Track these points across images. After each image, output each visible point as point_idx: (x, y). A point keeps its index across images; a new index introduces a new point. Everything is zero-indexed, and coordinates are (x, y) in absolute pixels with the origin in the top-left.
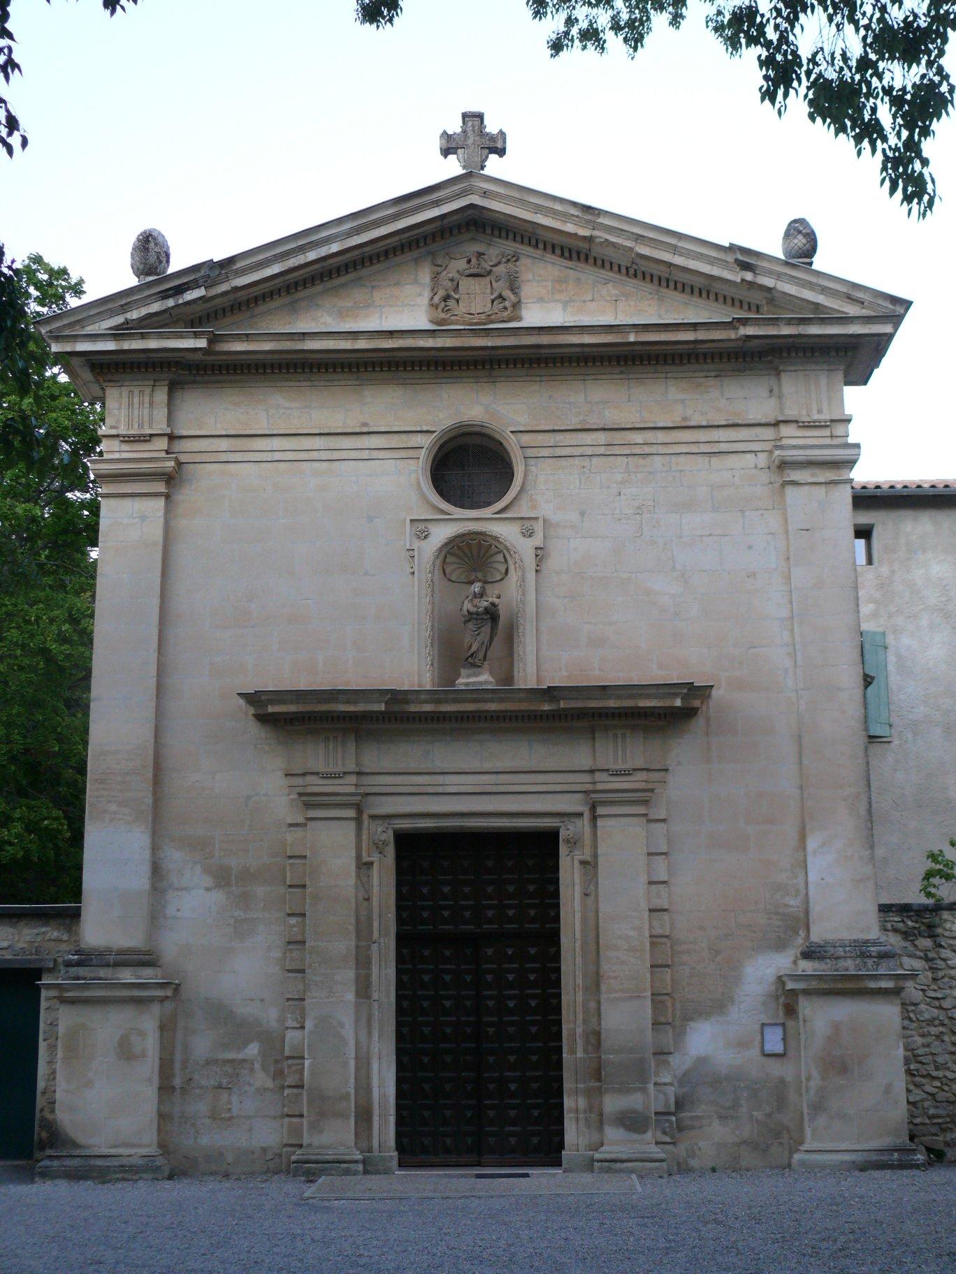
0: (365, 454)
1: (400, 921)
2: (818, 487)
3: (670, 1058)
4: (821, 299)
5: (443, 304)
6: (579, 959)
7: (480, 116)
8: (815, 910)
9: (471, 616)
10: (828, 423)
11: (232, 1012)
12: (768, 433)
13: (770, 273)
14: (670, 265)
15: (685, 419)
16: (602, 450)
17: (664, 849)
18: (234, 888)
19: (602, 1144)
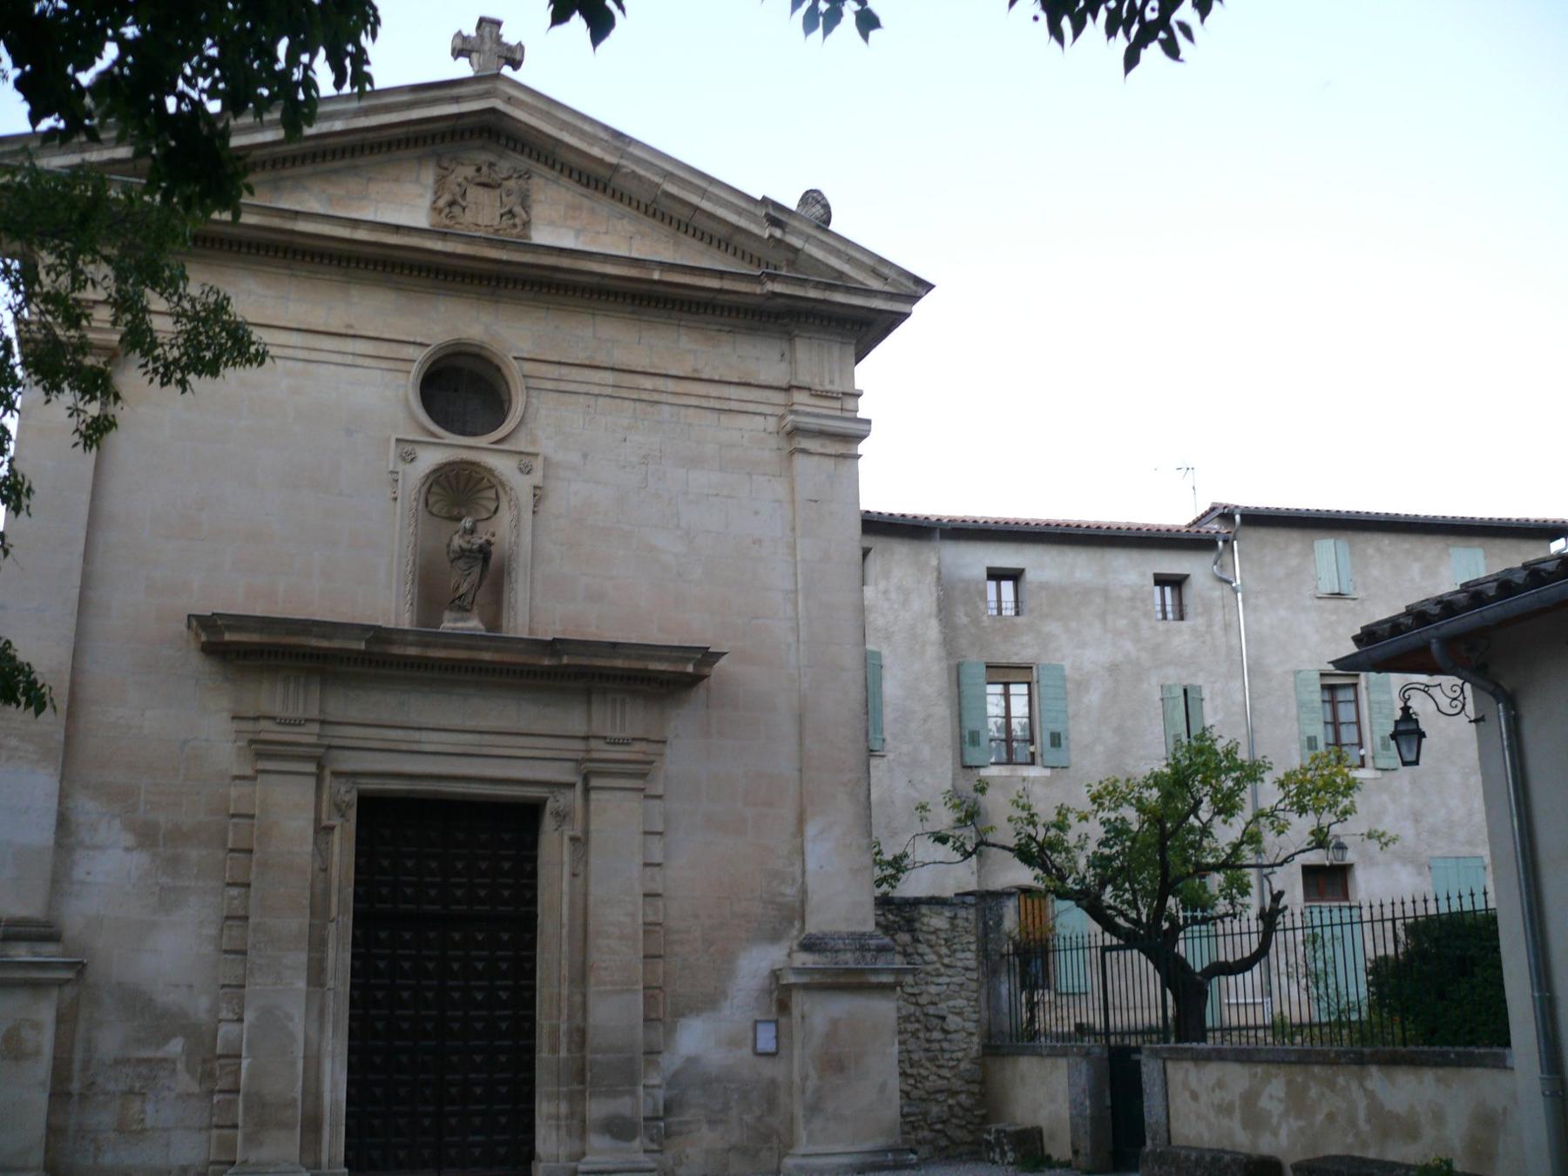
0: (349, 359)
1: (357, 898)
2: (827, 459)
3: (660, 1059)
4: (846, 268)
5: (447, 210)
6: (565, 947)
7: (498, 24)
8: (814, 900)
9: (463, 553)
10: (840, 395)
11: (151, 1000)
12: (779, 398)
13: (800, 234)
14: (696, 208)
15: (695, 370)
16: (609, 391)
17: (660, 828)
18: (161, 849)
19: (584, 1154)
